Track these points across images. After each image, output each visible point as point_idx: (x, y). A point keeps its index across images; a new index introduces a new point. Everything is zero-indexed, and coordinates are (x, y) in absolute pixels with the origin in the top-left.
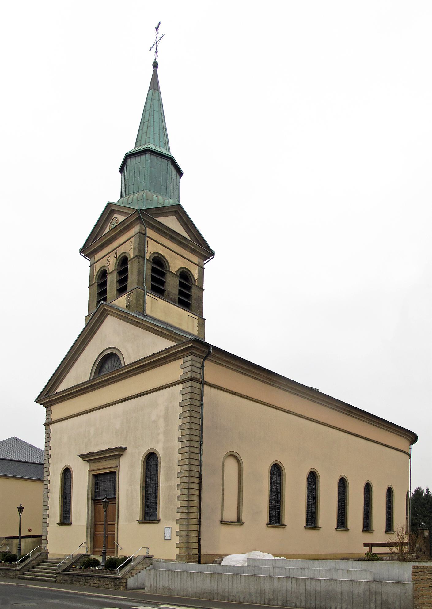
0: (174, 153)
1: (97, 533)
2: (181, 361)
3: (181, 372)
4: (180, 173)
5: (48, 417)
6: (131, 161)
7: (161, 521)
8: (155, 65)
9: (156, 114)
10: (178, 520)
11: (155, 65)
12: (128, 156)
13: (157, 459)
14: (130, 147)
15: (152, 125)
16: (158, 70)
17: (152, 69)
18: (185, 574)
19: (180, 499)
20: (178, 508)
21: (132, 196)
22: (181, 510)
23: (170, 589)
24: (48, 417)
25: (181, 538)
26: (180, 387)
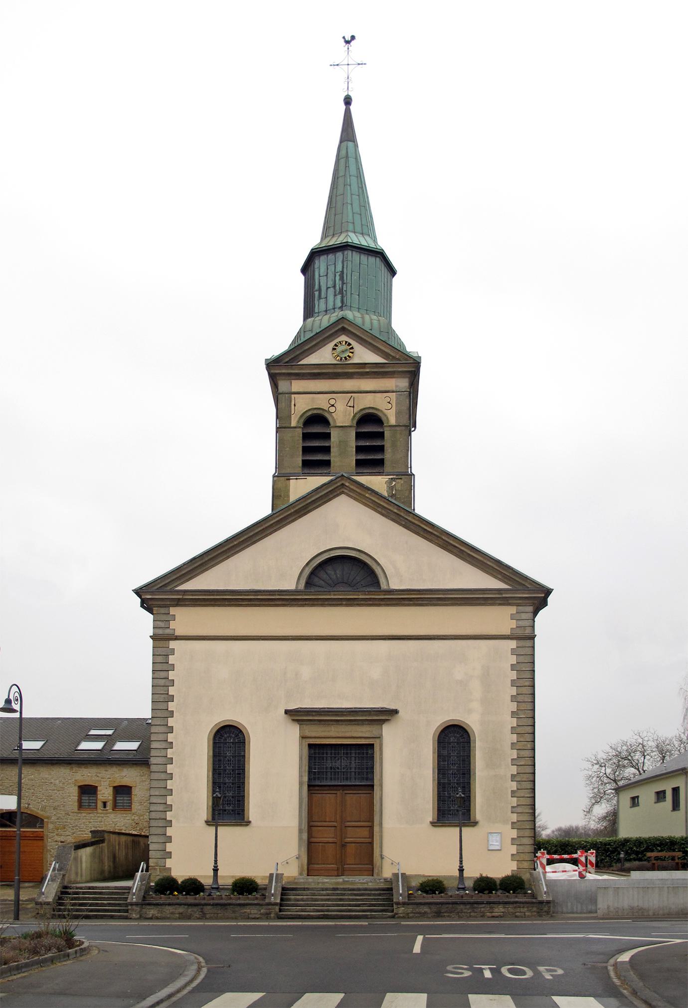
0: (385, 241)
1: (313, 840)
2: (513, 610)
3: (514, 624)
4: (393, 272)
5: (160, 659)
6: (321, 263)
7: (480, 823)
8: (348, 101)
9: (354, 180)
10: (513, 823)
11: (348, 101)
12: (315, 254)
13: (469, 742)
14: (314, 238)
15: (349, 202)
16: (351, 107)
17: (344, 107)
18: (666, 889)
19: (517, 795)
20: (513, 807)
21: (320, 318)
22: (520, 810)
23: (642, 909)
24: (160, 659)
25: (521, 847)
26: (513, 644)
